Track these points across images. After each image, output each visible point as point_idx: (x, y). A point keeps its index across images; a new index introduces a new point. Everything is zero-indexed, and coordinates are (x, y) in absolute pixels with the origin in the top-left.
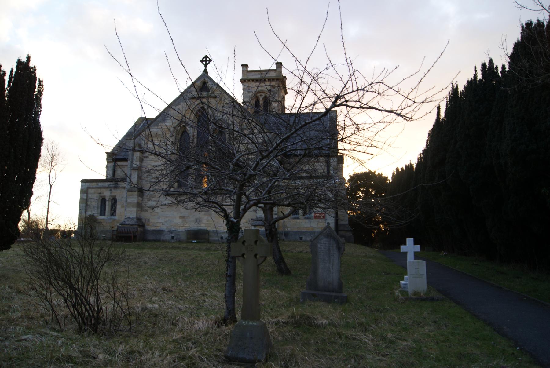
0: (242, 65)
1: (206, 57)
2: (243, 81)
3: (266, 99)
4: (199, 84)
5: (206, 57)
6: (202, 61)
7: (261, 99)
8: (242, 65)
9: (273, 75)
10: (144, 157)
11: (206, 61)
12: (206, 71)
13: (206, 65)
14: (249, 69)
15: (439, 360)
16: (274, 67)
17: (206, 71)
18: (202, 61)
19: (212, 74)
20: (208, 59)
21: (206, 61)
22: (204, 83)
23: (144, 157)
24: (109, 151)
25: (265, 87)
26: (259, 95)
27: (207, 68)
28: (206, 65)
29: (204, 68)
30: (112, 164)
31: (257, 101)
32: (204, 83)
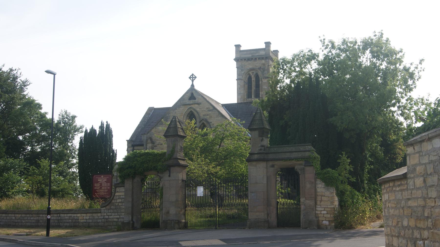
0: (235, 46)
1: (193, 75)
2: (236, 60)
3: (257, 76)
4: (189, 95)
5: (193, 75)
6: (190, 78)
7: (253, 76)
8: (235, 46)
9: (263, 53)
10: (154, 146)
11: (193, 78)
12: (193, 85)
13: (193, 81)
14: (242, 49)
15: (4, 82)
16: (263, 46)
17: (193, 85)
18: (190, 78)
19: (196, 87)
20: (194, 76)
21: (193, 78)
22: (192, 94)
23: (154, 146)
24: (128, 139)
25: (258, 64)
26: (251, 73)
27: (194, 83)
28: (193, 81)
29: (191, 83)
30: (132, 148)
31: (250, 78)
32: (192, 94)
